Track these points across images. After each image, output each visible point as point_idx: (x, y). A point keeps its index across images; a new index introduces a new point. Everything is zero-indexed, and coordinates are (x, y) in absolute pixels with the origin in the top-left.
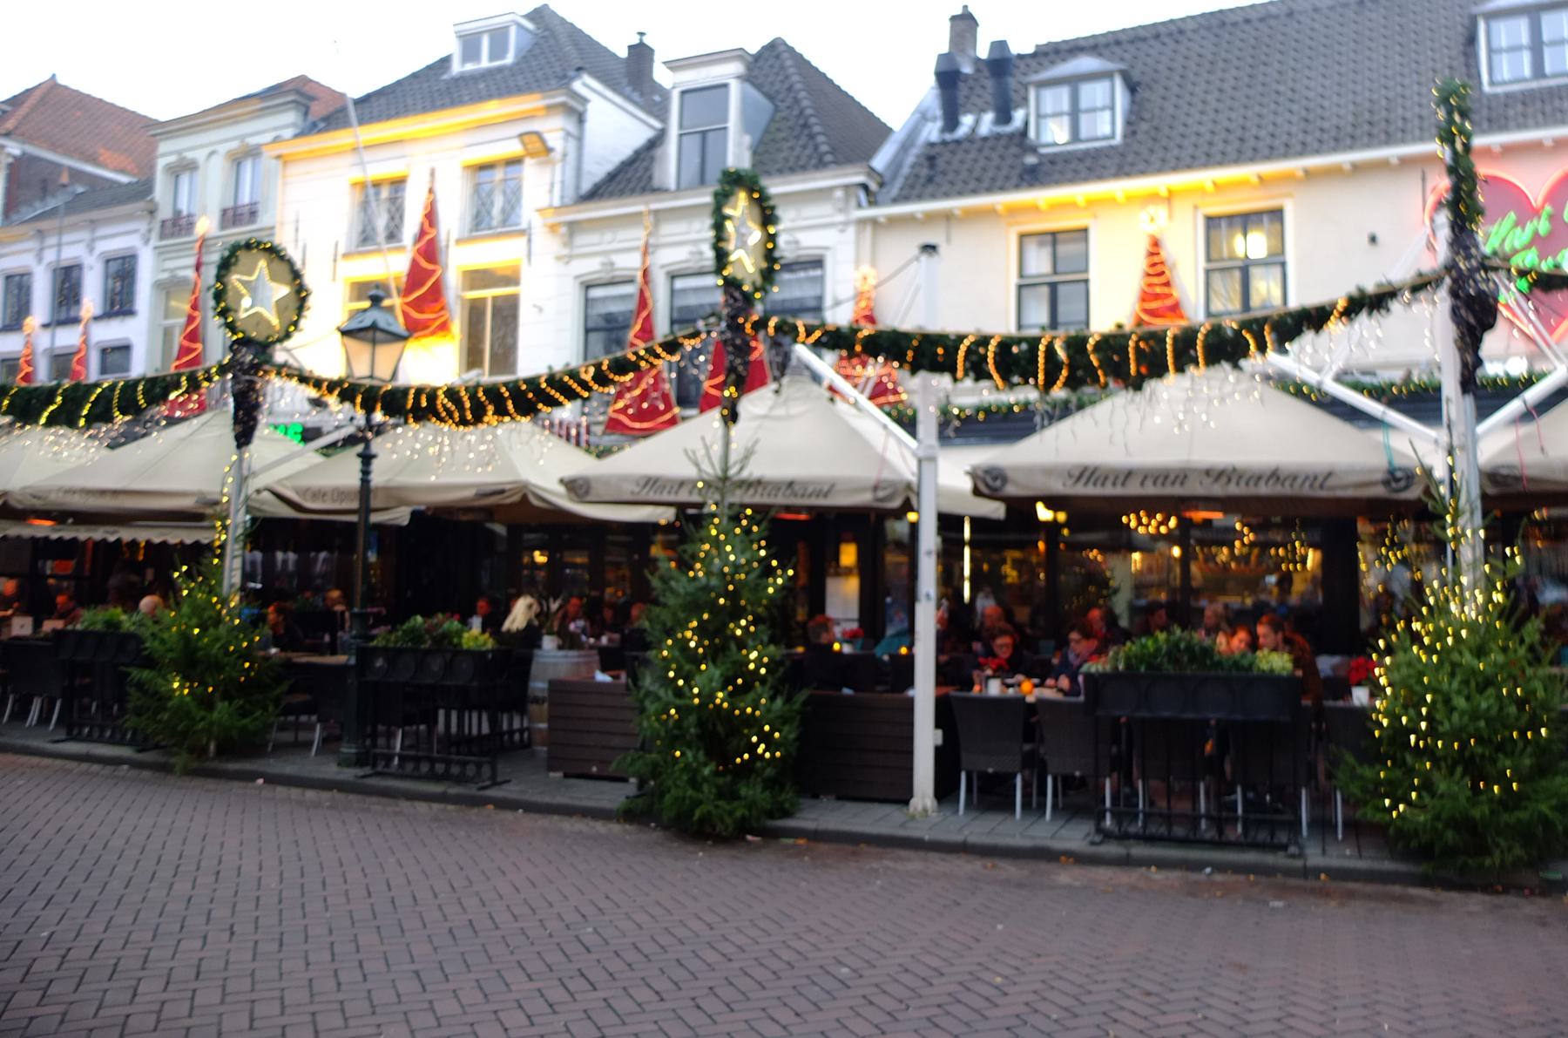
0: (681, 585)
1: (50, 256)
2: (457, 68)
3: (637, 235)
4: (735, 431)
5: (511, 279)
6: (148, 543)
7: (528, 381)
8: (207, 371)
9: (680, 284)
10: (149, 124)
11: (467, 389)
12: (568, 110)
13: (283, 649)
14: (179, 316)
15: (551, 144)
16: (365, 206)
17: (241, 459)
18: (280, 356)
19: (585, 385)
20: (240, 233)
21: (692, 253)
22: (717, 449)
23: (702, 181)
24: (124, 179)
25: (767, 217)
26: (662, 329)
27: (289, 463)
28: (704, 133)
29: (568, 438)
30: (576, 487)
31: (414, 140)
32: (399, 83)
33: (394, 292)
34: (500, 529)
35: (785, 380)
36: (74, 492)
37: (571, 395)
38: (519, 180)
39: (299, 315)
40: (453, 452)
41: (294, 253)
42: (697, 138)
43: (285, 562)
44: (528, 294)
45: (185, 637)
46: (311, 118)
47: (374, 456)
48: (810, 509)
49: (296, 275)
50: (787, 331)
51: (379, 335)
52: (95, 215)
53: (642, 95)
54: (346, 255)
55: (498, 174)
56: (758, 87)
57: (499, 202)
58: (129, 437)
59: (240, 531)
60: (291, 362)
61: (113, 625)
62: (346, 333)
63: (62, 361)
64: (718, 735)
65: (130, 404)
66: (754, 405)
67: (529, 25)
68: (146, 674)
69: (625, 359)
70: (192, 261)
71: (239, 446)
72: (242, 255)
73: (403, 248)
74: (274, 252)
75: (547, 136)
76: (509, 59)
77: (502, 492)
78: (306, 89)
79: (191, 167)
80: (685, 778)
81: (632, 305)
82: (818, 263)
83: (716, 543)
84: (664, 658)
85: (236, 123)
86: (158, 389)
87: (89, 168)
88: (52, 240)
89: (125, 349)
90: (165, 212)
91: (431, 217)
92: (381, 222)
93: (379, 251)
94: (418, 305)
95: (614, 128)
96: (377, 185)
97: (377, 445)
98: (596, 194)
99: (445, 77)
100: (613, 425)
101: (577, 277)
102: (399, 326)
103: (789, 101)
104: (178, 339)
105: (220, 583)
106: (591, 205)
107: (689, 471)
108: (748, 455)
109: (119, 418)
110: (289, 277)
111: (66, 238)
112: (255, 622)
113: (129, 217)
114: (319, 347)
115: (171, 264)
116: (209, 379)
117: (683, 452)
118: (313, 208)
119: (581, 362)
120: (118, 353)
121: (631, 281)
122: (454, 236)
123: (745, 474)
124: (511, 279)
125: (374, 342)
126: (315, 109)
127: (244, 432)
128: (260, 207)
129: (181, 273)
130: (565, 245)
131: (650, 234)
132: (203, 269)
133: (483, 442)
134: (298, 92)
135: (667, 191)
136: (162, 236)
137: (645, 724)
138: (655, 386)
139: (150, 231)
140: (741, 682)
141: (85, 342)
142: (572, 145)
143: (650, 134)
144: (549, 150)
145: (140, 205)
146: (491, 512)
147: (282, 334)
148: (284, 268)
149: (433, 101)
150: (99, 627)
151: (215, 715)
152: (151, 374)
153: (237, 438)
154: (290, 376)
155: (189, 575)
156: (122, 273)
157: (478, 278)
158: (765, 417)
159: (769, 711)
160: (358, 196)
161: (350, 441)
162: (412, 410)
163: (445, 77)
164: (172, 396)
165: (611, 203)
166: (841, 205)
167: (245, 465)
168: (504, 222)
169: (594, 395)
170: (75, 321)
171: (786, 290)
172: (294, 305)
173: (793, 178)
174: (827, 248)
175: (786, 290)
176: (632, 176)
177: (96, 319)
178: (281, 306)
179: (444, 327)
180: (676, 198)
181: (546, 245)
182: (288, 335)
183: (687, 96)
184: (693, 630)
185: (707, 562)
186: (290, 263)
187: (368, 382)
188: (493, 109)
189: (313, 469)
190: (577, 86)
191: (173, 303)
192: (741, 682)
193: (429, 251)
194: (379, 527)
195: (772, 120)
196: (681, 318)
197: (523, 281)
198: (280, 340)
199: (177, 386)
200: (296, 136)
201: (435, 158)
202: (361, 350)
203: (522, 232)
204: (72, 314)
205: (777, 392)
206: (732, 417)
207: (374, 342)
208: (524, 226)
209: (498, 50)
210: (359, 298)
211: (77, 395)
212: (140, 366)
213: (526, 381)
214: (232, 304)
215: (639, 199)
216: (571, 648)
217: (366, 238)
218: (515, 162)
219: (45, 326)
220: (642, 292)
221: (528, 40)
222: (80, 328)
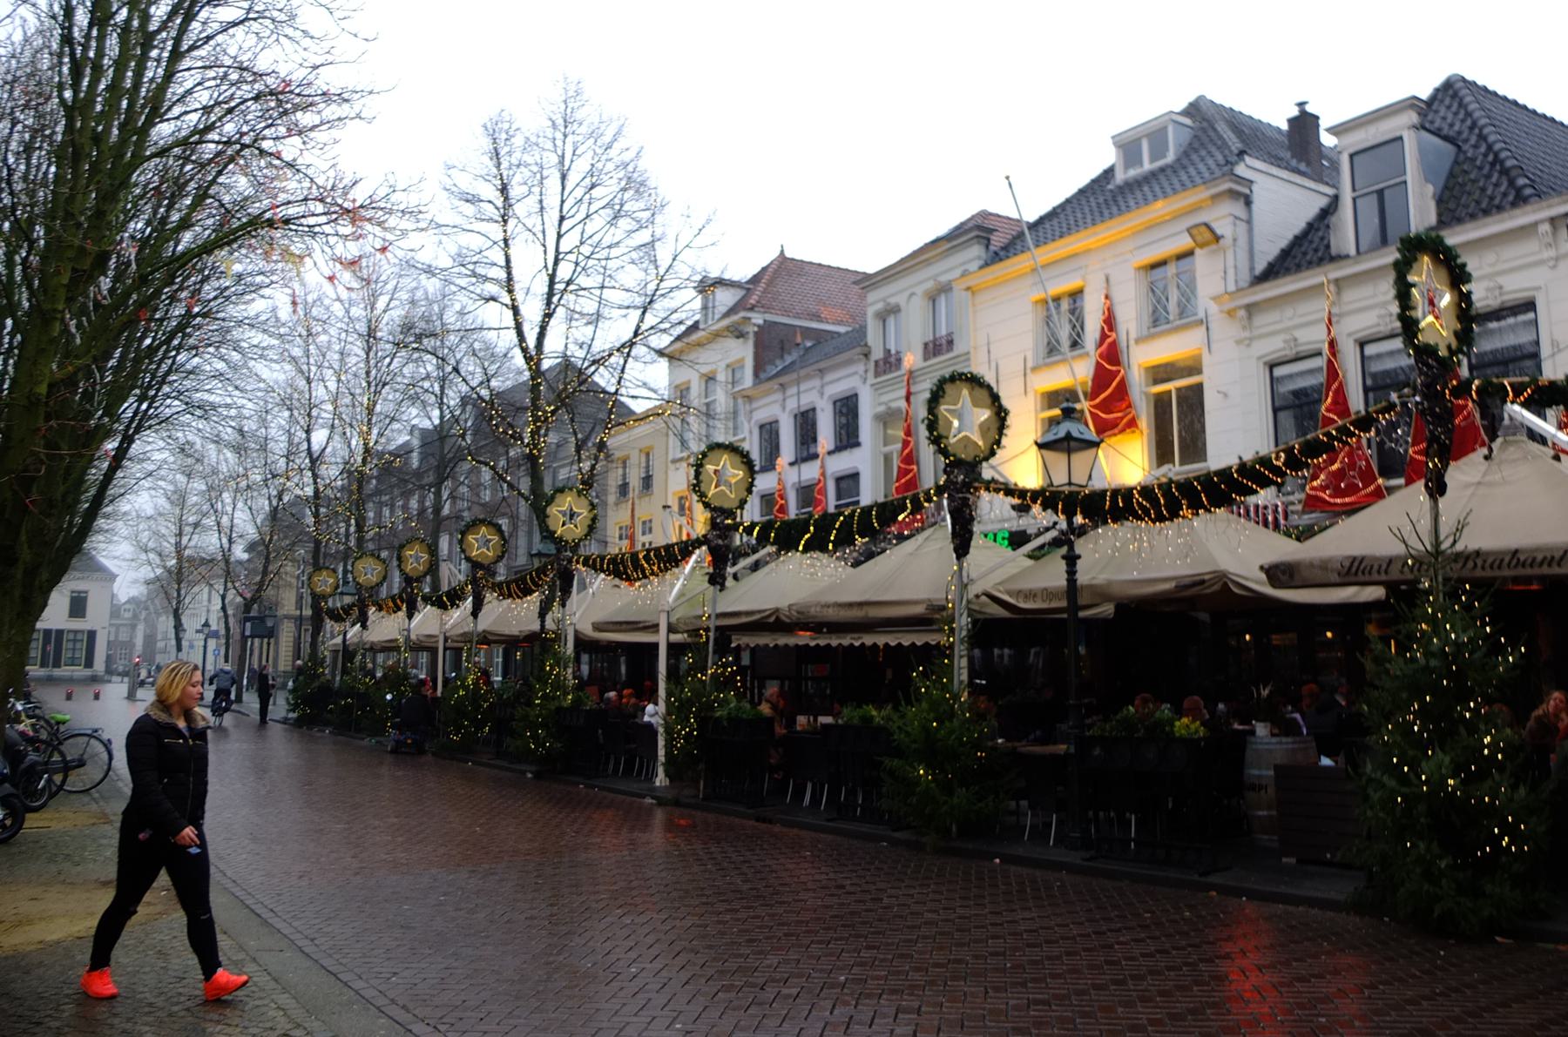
0: (1396, 668)
1: (792, 404)
2: (1120, 177)
3: (1318, 308)
4: (1442, 502)
5: (1194, 368)
6: (887, 645)
7: (1220, 473)
8: (927, 493)
9: (1370, 350)
10: (867, 282)
11: (1160, 486)
12: (1233, 194)
13: (1008, 740)
14: (894, 443)
15: (1219, 232)
16: (1048, 320)
17: (961, 569)
18: (987, 473)
19: (1277, 471)
20: (943, 366)
21: (1380, 317)
22: (1425, 525)
23: (1384, 241)
24: (842, 329)
25: (1458, 276)
26: (1356, 402)
27: (997, 569)
28: (1380, 193)
29: (1266, 524)
30: (1279, 573)
31: (1088, 251)
32: (1068, 201)
33: (1082, 397)
34: (1204, 616)
35: (1496, 445)
37: (1265, 483)
38: (1192, 272)
39: (1001, 434)
40: (1151, 546)
41: (990, 378)
42: (1374, 198)
43: (1001, 657)
44: (1213, 381)
45: (926, 729)
46: (992, 248)
47: (1079, 557)
48: (1542, 579)
49: (995, 398)
50: (1492, 397)
51: (1073, 444)
52: (822, 365)
53: (1308, 164)
54: (1034, 369)
55: (1171, 269)
56: (1437, 133)
57: (1174, 296)
58: (870, 556)
59: (964, 633)
60: (997, 477)
61: (867, 720)
62: (1041, 446)
63: (808, 493)
64: (1454, 824)
65: (859, 529)
66: (1463, 474)
67: (1188, 121)
68: (896, 762)
69: (1317, 439)
70: (903, 392)
71: (959, 558)
72: (948, 388)
73: (1087, 354)
74: (975, 381)
75: (1214, 225)
76: (1170, 157)
77: (1203, 582)
78: (987, 224)
79: (894, 310)
80: (1418, 870)
81: (1321, 378)
82: (1530, 306)
83: (1432, 620)
84: (1386, 744)
86: (887, 511)
87: (814, 325)
88: (793, 390)
89: (854, 477)
90: (877, 354)
91: (1110, 321)
92: (1064, 333)
93: (1064, 361)
94: (1105, 406)
95: (1284, 204)
96: (1057, 299)
97: (1081, 546)
98: (1272, 272)
99: (1110, 187)
100: (1312, 503)
101: (1259, 358)
102: (1092, 435)
103: (1473, 139)
104: (896, 463)
105: (951, 680)
106: (1266, 285)
107: (1398, 549)
108: (1460, 529)
109: (859, 540)
110: (988, 401)
111: (803, 387)
112: (980, 717)
113: (849, 362)
114: (1022, 464)
115: (885, 398)
116: (929, 500)
117: (1390, 526)
118: (1005, 339)
119: (1272, 448)
120: (848, 482)
121: (1319, 354)
122: (1133, 336)
123: (1459, 547)
124: (1194, 368)
125: (1069, 452)
126: (989, 239)
127: (962, 545)
128: (955, 337)
129: (894, 405)
130: (1244, 328)
131: (1333, 303)
132: (912, 399)
133: (1180, 535)
134: (979, 227)
135: (1347, 257)
136: (877, 375)
137: (1369, 813)
138: (1352, 465)
140: (1475, 770)
141: (823, 474)
142: (1242, 227)
143: (1323, 202)
144: (1217, 238)
145: (858, 350)
146: (1193, 602)
147: (987, 452)
148: (984, 394)
149: (1101, 214)
150: (855, 721)
151: (956, 800)
152: (881, 499)
153: (956, 550)
154: (997, 491)
155: (925, 675)
156: (847, 408)
157: (1160, 373)
158: (1479, 483)
159: (1511, 800)
160: (1042, 313)
161: (1056, 543)
162: (1109, 511)
163: (1110, 187)
164: (900, 518)
165: (1289, 279)
166: (1550, 239)
167: (965, 574)
168: (1181, 314)
169: (1289, 479)
170: (815, 456)
171: (1491, 341)
172: (995, 426)
173: (1489, 220)
174: (1538, 288)
175: (1491, 341)
176: (1308, 250)
177: (830, 453)
178: (984, 429)
179: (1132, 424)
180: (1357, 263)
181: (1225, 330)
182: (993, 453)
184: (1414, 713)
185: (1425, 640)
186: (989, 388)
187: (1066, 489)
188: (1160, 208)
189: (1023, 573)
190: (1241, 170)
191: (890, 432)
192: (1475, 770)
193: (1111, 354)
194: (1086, 620)
195: (1456, 162)
196: (1377, 386)
198: (986, 459)
199: (904, 509)
200: (981, 268)
201: (1108, 270)
202: (1058, 460)
204: (812, 451)
205: (1487, 458)
206: (1437, 488)
207: (1069, 452)
208: (1201, 315)
209: (1158, 151)
210: (1050, 407)
211: (826, 521)
212: (870, 493)
213: (1217, 473)
214: (944, 433)
215: (1318, 270)
216: (1287, 735)
217: (1052, 349)
218: (1188, 254)
219: (791, 464)
220: (1330, 362)
221: (1186, 135)
222: (818, 462)
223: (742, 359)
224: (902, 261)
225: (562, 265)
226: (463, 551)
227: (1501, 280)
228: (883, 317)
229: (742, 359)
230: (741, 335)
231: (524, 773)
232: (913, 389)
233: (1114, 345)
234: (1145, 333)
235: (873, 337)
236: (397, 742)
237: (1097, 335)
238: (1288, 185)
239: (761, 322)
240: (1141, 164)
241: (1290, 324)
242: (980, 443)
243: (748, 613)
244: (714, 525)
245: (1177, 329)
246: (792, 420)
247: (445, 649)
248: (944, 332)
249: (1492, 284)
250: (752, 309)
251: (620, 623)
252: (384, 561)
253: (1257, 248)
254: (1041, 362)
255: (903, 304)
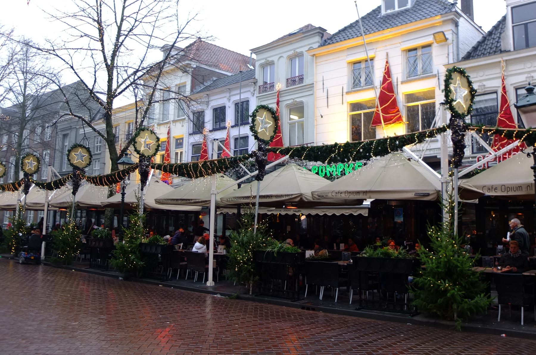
1: (236, 98)
2: (383, 12)
3: (496, 72)
15: (447, 36)
28: (526, 25)
36: (341, 193)
54: (347, 93)
70: (276, 101)
75: (446, 33)
76: (409, 6)
79: (272, 64)
85: (291, 44)
87: (217, 71)
90: (260, 83)
91: (388, 73)
106: (467, 62)
122: (400, 80)
132: (280, 103)
135: (509, 51)
139: (254, 91)
141: (228, 136)
142: (455, 36)
144: (447, 39)
145: (252, 80)
157: (410, 97)
168: (424, 71)
170: (225, 128)
177: (232, 127)
183: (514, 9)
197: (436, 97)
203: (435, 76)
204: (222, 125)
208: (435, 72)
218: (429, 46)
222: (227, 130)
223: (185, 82)
224: (280, 40)
225: (125, 22)
226: (69, 160)
227: (484, 83)
228: (263, 66)
229: (185, 82)
230: (185, 71)
231: (117, 277)
232: (280, 100)
233: (391, 84)
234: (405, 79)
235: (258, 74)
236: (26, 258)
237: (381, 79)
238: (466, 22)
239: (195, 66)
240: (394, 9)
241: (482, 78)
242: (464, 106)
243: (277, 196)
244: (260, 149)
245: (423, 78)
246: (212, 111)
247: (48, 210)
248: (297, 75)
249: (481, 84)
250: (191, 60)
251: (177, 200)
252: (5, 166)
253: (461, 46)
254: (405, 79)
255: (276, 61)
